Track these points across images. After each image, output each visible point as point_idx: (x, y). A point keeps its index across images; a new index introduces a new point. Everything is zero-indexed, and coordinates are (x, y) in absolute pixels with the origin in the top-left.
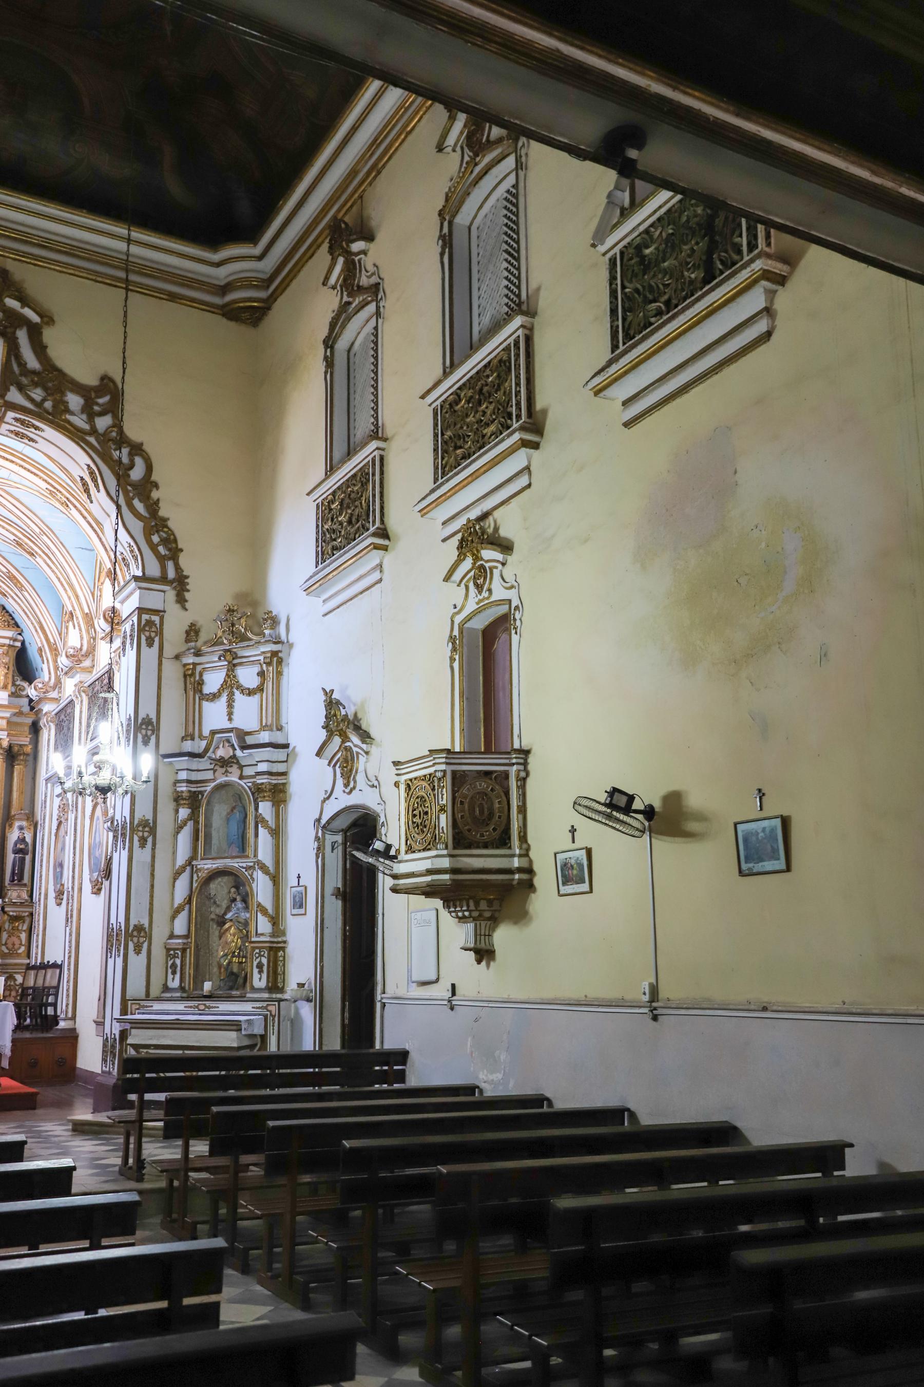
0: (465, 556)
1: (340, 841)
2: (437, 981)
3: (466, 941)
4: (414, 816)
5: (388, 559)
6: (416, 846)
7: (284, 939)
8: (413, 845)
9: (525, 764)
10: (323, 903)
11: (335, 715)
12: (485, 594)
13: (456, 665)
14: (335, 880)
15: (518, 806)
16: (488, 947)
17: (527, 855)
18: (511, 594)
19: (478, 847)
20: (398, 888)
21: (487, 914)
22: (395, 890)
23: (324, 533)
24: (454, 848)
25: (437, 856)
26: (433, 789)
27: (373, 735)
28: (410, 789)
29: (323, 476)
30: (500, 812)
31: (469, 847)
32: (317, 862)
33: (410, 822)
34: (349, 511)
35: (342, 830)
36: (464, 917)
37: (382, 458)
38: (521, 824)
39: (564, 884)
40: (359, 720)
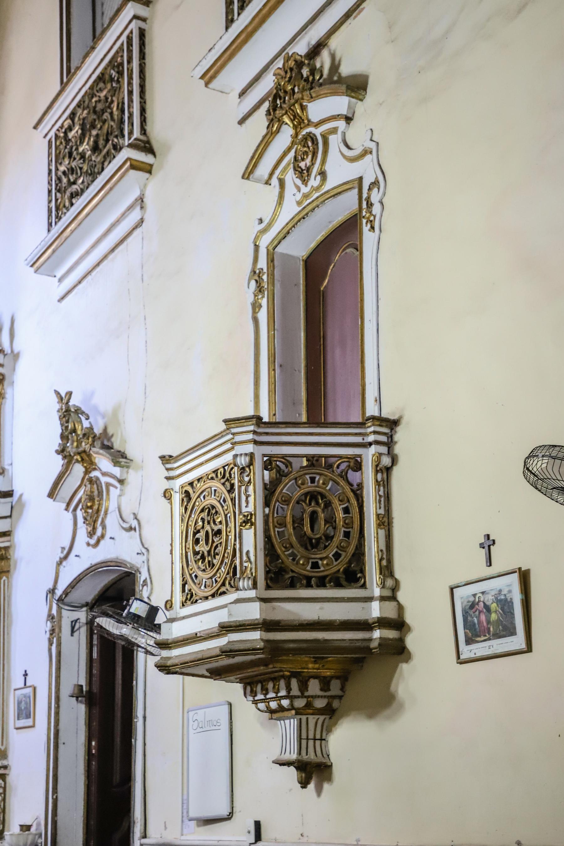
0: (281, 123)
1: (83, 620)
2: (230, 817)
3: (283, 750)
4: (197, 542)
5: (154, 187)
6: (199, 592)
7: (5, 763)
8: (195, 589)
9: (390, 444)
10: (58, 707)
11: (74, 431)
12: (314, 181)
13: (263, 315)
14: (76, 674)
15: (378, 515)
16: (320, 759)
17: (393, 598)
18: (366, 169)
19: (309, 585)
20: (169, 663)
21: (320, 704)
22: (165, 668)
23: (59, 179)
24: (268, 587)
25: (238, 601)
26: (231, 490)
27: (130, 453)
28: (190, 499)
29: (58, 87)
30: (346, 525)
31: (292, 585)
32: (50, 650)
33: (191, 554)
34: (94, 132)
35: (87, 605)
36: (281, 709)
37: (142, 34)
38: (383, 546)
39: (469, 641)
40: (109, 438)
